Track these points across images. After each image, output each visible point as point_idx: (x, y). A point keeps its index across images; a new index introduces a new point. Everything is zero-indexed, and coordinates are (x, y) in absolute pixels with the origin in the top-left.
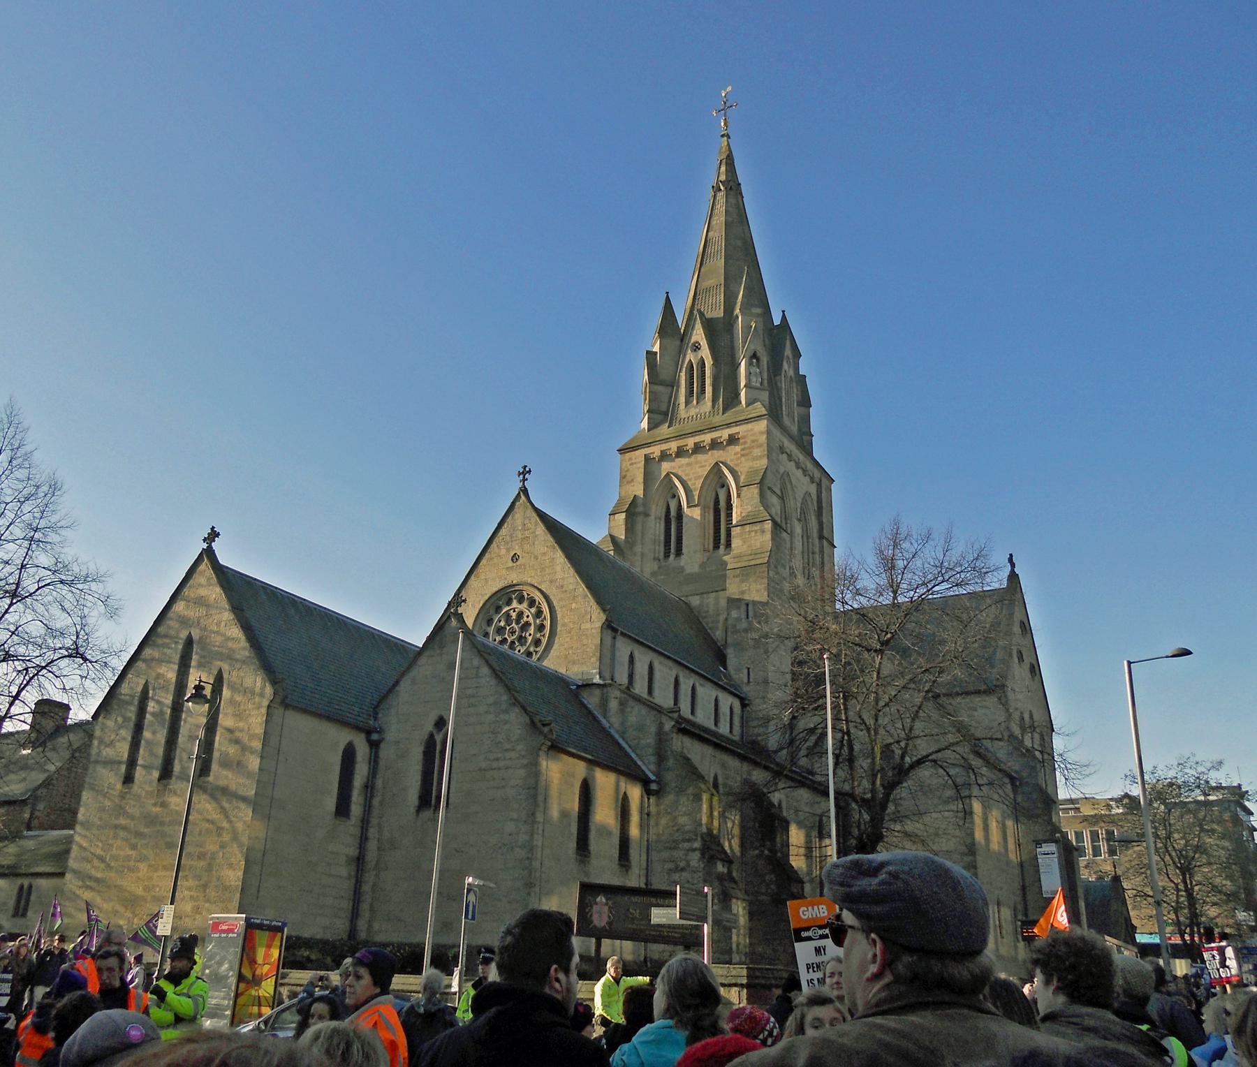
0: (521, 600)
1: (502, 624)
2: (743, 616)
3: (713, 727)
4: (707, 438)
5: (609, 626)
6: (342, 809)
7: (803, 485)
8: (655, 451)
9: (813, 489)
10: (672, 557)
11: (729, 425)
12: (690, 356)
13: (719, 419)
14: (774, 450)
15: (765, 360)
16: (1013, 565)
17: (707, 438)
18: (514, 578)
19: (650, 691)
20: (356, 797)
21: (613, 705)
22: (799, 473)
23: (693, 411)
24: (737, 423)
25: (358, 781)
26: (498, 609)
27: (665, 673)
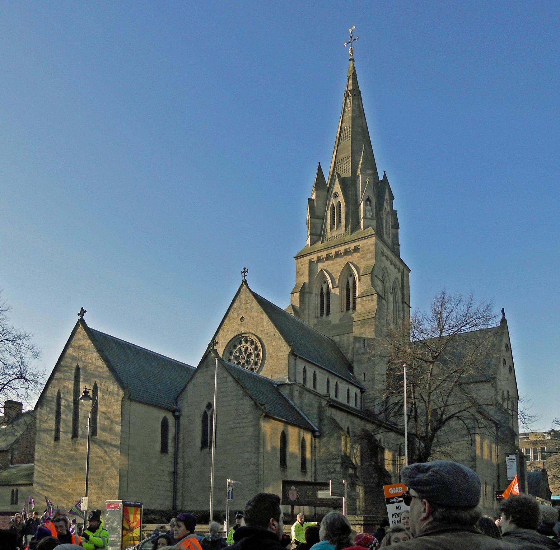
0: (246, 341)
1: (238, 354)
2: (362, 346)
3: (347, 404)
4: (342, 249)
5: (293, 354)
6: (164, 449)
7: (394, 274)
8: (315, 257)
9: (399, 276)
10: (325, 316)
11: (354, 241)
12: (333, 201)
13: (348, 238)
14: (379, 254)
15: (374, 202)
16: (504, 314)
17: (342, 249)
18: (242, 330)
19: (315, 386)
20: (170, 443)
21: (296, 394)
22: (392, 267)
23: (335, 233)
24: (359, 239)
25: (171, 435)
26: (235, 346)
27: (322, 377)
